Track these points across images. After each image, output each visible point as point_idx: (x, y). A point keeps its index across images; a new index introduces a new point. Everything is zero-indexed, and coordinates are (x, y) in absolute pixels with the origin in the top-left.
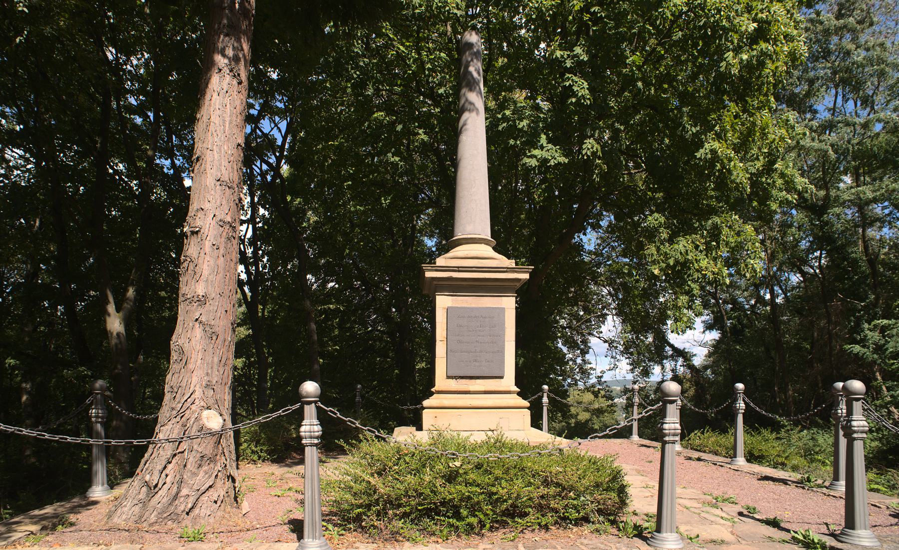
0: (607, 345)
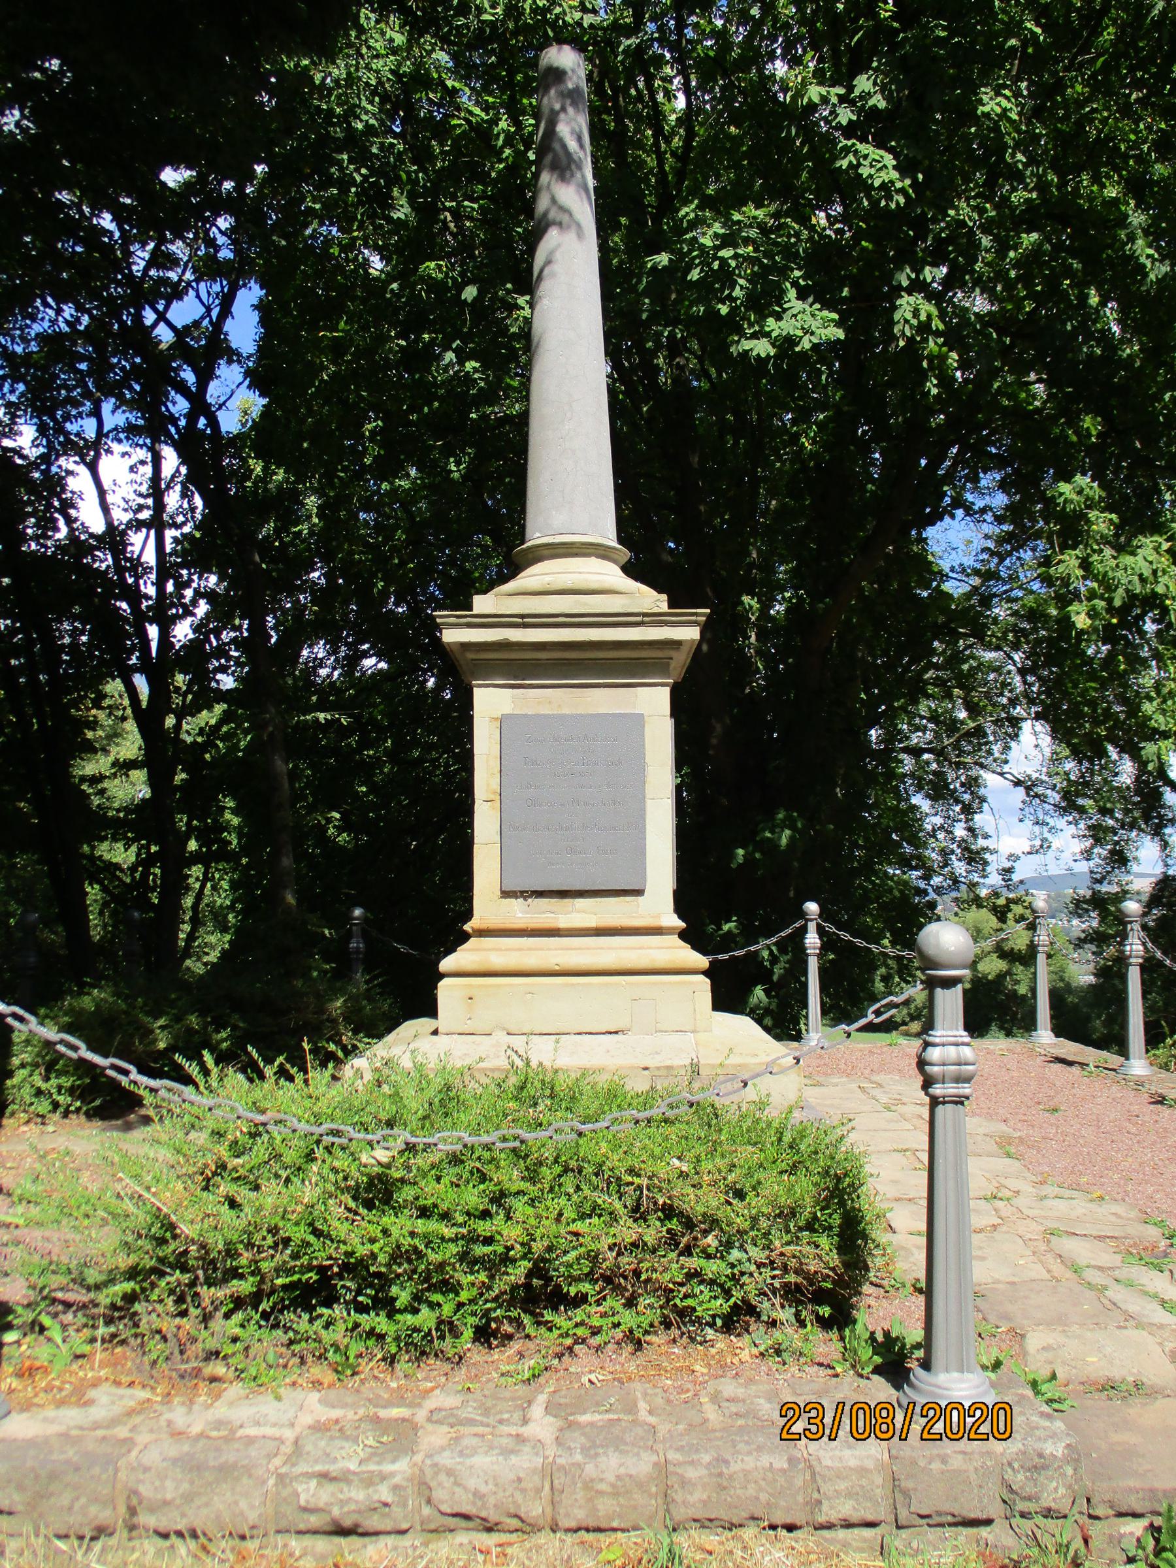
0: (1021, 791)
